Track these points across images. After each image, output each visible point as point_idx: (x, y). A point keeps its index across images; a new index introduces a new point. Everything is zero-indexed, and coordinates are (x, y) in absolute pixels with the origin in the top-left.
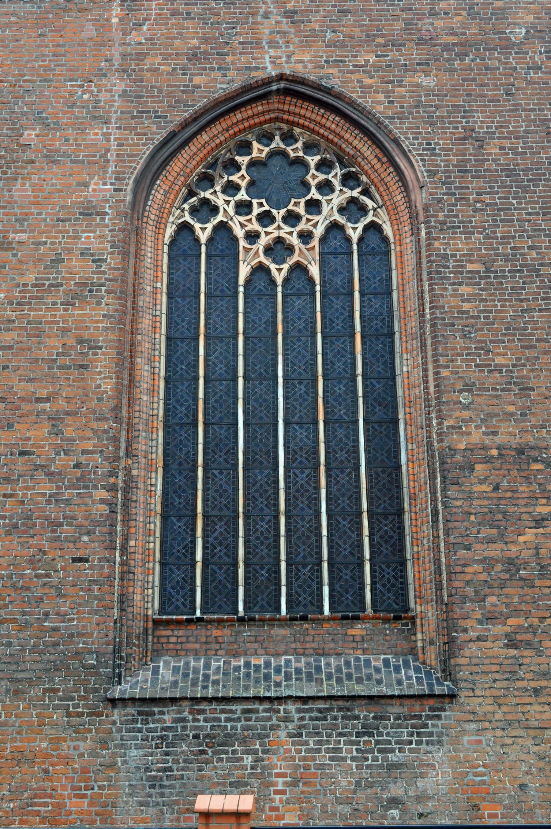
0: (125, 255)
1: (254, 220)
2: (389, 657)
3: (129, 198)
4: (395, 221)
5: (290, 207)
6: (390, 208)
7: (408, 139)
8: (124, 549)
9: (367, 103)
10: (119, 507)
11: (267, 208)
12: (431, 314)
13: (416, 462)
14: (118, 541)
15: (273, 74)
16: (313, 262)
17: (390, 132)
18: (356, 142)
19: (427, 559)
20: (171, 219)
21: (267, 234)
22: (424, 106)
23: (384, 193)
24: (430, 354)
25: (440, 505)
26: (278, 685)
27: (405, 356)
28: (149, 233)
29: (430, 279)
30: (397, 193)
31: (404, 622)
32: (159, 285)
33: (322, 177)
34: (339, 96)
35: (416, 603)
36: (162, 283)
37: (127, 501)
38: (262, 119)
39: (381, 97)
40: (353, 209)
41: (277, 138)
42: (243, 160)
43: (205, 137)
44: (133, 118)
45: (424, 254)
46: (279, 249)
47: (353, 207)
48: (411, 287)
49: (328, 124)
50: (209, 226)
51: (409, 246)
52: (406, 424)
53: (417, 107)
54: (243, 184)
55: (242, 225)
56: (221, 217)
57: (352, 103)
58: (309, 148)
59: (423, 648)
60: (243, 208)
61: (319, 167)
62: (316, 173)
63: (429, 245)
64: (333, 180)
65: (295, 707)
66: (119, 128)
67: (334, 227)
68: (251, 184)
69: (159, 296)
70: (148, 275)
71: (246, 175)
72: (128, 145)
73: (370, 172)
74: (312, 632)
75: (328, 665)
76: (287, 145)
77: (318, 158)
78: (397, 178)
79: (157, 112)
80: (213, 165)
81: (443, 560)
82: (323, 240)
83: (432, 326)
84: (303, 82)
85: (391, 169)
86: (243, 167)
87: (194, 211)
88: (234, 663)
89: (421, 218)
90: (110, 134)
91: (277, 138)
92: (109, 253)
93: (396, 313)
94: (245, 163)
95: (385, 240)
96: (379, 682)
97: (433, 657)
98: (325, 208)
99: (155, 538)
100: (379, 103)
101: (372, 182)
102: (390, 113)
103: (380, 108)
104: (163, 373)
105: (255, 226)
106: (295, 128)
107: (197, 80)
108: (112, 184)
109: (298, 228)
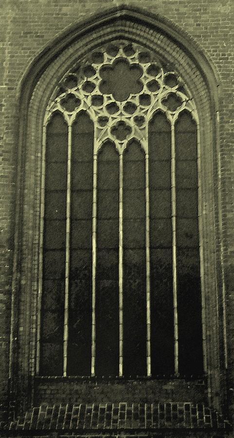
0: (17, 135)
1: (104, 109)
2: (189, 403)
3: (18, 95)
4: (200, 110)
5: (129, 100)
6: (197, 100)
7: (210, 51)
8: (16, 333)
9: (181, 25)
10: (12, 305)
11: (113, 100)
12: (222, 175)
13: (210, 276)
14: (12, 328)
15: (118, 5)
16: (144, 138)
17: (198, 46)
18: (174, 54)
19: (215, 339)
20: (48, 108)
21: (113, 118)
22: (221, 28)
23: (193, 90)
24: (220, 202)
25: (224, 304)
26: (115, 421)
27: (204, 204)
28: (33, 119)
29: (222, 151)
30: (202, 89)
31: (200, 380)
32: (39, 155)
33: (151, 78)
34: (163, 21)
35: (208, 368)
36: (41, 153)
37: (18, 302)
38: (110, 37)
39: (191, 21)
40: (172, 100)
41: (121, 50)
42: (97, 66)
43: (71, 50)
44: (20, 37)
45: (218, 133)
46: (121, 129)
47: (173, 100)
48: (209, 156)
49: (155, 41)
50: (74, 113)
51: (209, 127)
52: (204, 250)
53: (216, 28)
54: (97, 83)
55: (97, 113)
56: (81, 107)
57: (171, 26)
58: (143, 57)
59: (212, 398)
60: (97, 100)
61: (149, 71)
62: (147, 75)
63: (222, 127)
64: (159, 80)
65: (126, 436)
66: (11, 45)
67: (159, 114)
68: (103, 83)
69: (39, 163)
70: (32, 148)
71: (99, 77)
72: (17, 56)
73: (184, 75)
74: (140, 387)
75: (149, 408)
76: (128, 56)
77: (149, 64)
78: (202, 79)
79: (37, 33)
80: (76, 70)
81: (225, 340)
82: (151, 123)
83: (223, 183)
84: (137, 10)
85: (198, 73)
86: (97, 71)
87: (64, 102)
88: (87, 407)
89: (217, 108)
90: (5, 49)
91: (121, 50)
92: (5, 133)
93: (199, 174)
94: (99, 68)
95: (194, 122)
96: (181, 420)
97: (218, 404)
98: (153, 101)
99: (37, 326)
100: (191, 25)
101: (185, 81)
102: (197, 33)
103: (191, 29)
104: (42, 215)
105: (105, 113)
106: (133, 43)
107: (65, 10)
108: (6, 84)
109: (135, 115)
